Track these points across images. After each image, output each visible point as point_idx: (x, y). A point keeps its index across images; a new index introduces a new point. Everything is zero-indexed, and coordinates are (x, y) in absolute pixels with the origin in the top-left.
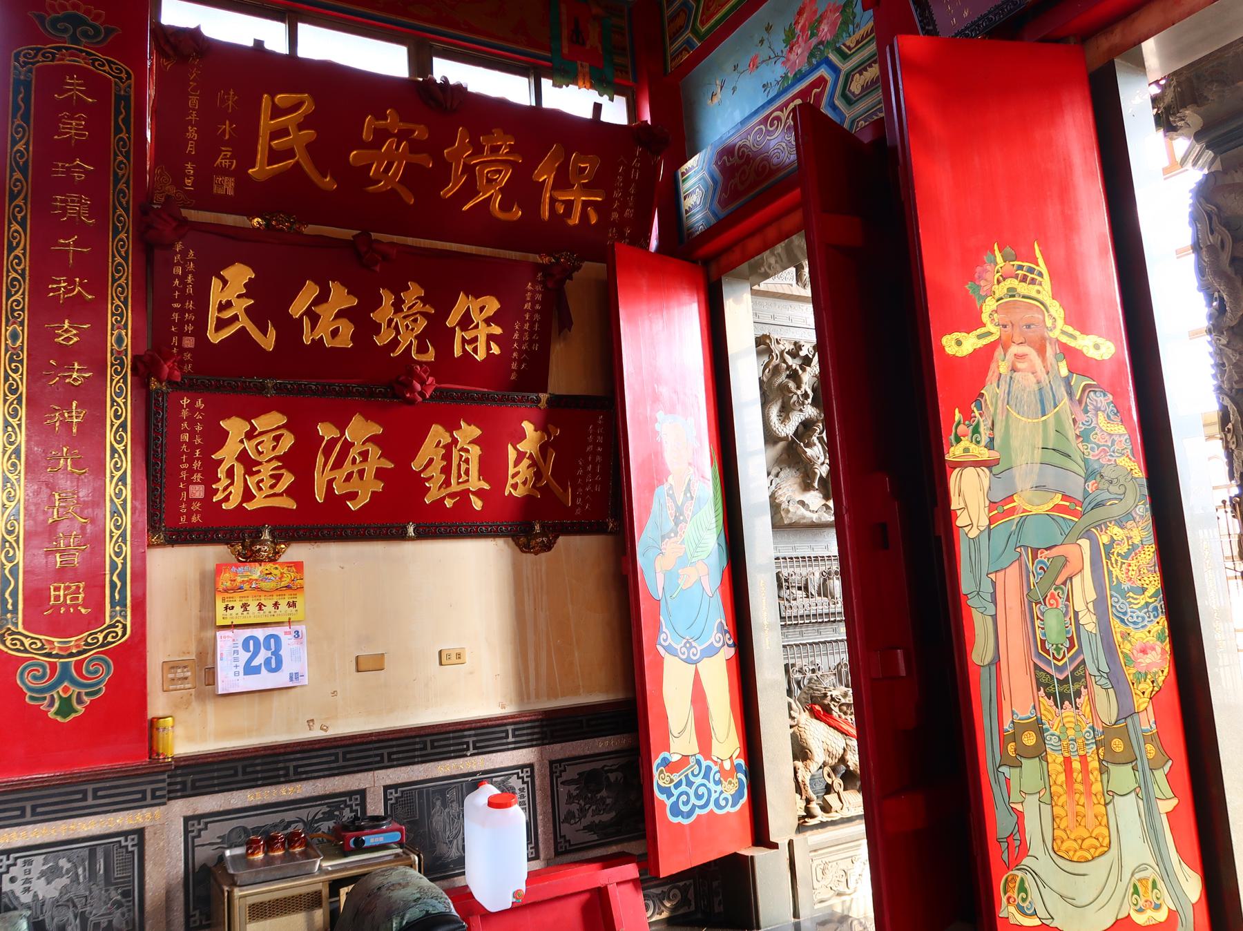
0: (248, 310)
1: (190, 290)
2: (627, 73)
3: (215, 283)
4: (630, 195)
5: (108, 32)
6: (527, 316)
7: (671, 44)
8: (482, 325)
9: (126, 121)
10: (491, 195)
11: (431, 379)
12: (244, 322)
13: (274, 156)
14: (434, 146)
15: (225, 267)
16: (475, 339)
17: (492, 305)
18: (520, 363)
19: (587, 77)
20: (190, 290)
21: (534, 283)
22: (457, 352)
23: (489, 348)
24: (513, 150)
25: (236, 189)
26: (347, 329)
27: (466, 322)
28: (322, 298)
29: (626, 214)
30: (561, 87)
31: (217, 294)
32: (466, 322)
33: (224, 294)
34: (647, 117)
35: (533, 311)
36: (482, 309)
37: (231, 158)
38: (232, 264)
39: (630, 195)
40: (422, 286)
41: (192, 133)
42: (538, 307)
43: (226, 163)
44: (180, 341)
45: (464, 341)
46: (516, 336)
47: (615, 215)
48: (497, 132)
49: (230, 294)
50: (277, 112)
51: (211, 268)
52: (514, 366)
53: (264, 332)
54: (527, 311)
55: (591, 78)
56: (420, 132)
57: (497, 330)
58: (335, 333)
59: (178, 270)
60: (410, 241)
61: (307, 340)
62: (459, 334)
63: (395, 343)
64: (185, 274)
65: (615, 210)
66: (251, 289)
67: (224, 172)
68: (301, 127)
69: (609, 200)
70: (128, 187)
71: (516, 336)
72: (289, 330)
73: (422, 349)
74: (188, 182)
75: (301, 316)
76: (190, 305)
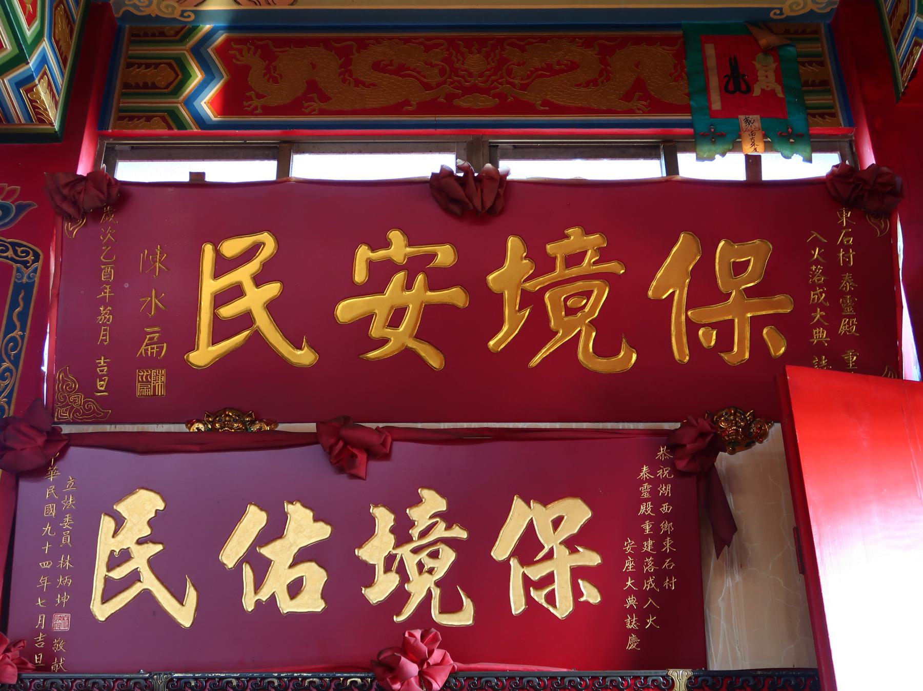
0: (153, 563)
1: (66, 539)
2: (833, 115)
3: (107, 524)
4: (843, 294)
5: (20, 209)
6: (647, 527)
7: (898, 49)
8: (561, 552)
9: (23, 317)
10: (575, 329)
11: (438, 655)
12: (149, 582)
13: (221, 329)
14: (471, 273)
15: (120, 499)
16: (549, 579)
17: (576, 513)
18: (642, 617)
19: (759, 135)
20: (66, 539)
21: (654, 466)
22: (517, 605)
23: (577, 592)
24: (604, 255)
25: (168, 385)
26: (315, 576)
27: (528, 550)
28: (275, 530)
29: (842, 329)
30: (712, 158)
31: (107, 542)
32: (528, 550)
33: (120, 537)
34: (870, 159)
35: (658, 517)
36: (557, 523)
37: (160, 341)
38: (131, 492)
39: (843, 294)
40: (442, 494)
41: (105, 315)
42: (665, 508)
43: (152, 350)
44: (49, 621)
45: (528, 583)
46: (629, 565)
47: (820, 334)
48: (574, 232)
49: (126, 539)
50: (223, 266)
51: (103, 503)
52: (631, 623)
53: (180, 598)
54: (645, 517)
55: (765, 136)
56: (445, 255)
57: (592, 559)
58: (295, 588)
59: (51, 510)
60: (419, 425)
61: (249, 604)
62: (516, 571)
63: (400, 596)
64: (61, 514)
65: (819, 324)
66: (159, 527)
67: (152, 363)
68: (259, 280)
69: (803, 308)
70: (9, 403)
71: (629, 565)
72: (219, 588)
73: (451, 605)
74: (101, 385)
75: (239, 566)
76: (65, 562)
